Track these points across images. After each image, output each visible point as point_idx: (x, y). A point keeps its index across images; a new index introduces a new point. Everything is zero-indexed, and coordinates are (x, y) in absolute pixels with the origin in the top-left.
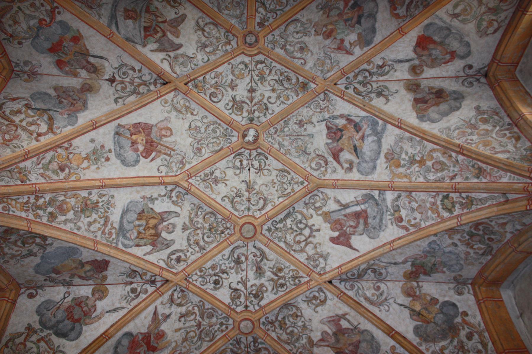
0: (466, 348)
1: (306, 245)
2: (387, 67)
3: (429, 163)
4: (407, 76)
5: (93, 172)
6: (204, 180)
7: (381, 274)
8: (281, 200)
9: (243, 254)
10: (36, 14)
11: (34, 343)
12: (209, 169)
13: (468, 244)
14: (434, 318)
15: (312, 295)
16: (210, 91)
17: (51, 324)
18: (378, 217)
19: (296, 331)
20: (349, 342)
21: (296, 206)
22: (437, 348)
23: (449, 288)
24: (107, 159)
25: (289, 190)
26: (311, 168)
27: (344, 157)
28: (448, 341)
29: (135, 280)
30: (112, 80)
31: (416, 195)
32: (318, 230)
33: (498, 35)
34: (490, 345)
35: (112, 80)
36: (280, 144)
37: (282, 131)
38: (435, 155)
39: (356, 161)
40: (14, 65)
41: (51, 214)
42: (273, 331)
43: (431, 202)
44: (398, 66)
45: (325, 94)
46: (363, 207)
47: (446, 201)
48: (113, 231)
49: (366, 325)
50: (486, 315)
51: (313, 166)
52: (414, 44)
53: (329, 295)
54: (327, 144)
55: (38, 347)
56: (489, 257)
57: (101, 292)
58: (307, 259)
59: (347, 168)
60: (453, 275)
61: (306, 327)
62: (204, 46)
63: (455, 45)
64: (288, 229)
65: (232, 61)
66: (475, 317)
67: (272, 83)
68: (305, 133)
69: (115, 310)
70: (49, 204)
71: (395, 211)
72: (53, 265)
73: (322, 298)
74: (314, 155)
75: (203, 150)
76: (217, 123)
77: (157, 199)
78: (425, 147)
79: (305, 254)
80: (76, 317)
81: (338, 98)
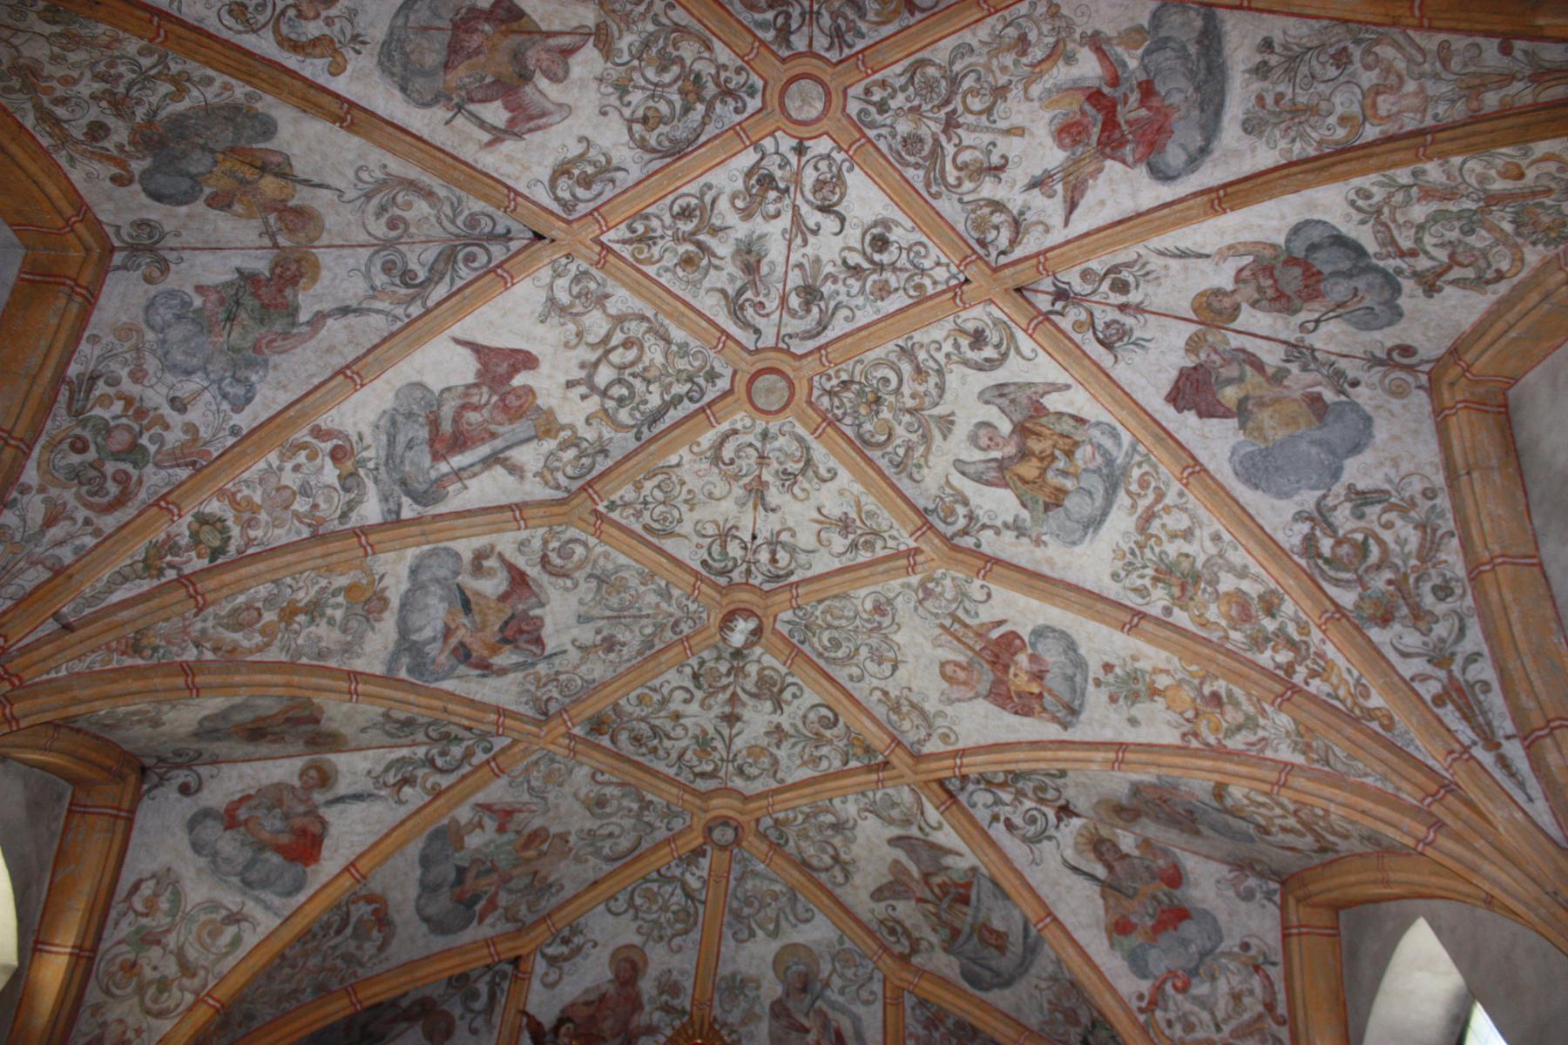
0: (104, 104)
1: (608, 337)
2: (391, 780)
3: (270, 616)
4: (340, 760)
5: (1148, 657)
6: (876, 534)
7: (388, 268)
8: (674, 459)
9: (793, 314)
10: (1188, 1006)
11: (1426, 253)
12: (861, 559)
13: (141, 413)
14: (216, 162)
15: (596, 188)
16: (835, 731)
17: (1370, 277)
18: (399, 449)
19: (651, 73)
20: (482, 58)
21: (633, 445)
22: (195, 93)
23: (178, 235)
24: (1108, 667)
25: (649, 485)
26: (585, 544)
27: (495, 581)
28: (163, 114)
29: (1114, 315)
30: (1065, 811)
31: (298, 532)
32: (570, 384)
33: (127, 879)
34: (29, 122)
35: (1065, 811)
36: (665, 594)
37: (660, 627)
38: (258, 639)
39: (466, 580)
40: (1277, 898)
41: (1271, 611)
42: (725, 67)
43: (257, 526)
44: (366, 785)
45: (545, 714)
46: (444, 468)
47: (217, 543)
48: (1134, 487)
49: (424, 121)
50: (54, 192)
51: (579, 551)
52: (327, 842)
53: (544, 198)
54: (542, 605)
55: (1418, 240)
56: (73, 370)
57: (1213, 311)
58: (607, 296)
59: (487, 557)
60: (171, 282)
61: (617, 87)
62: (838, 827)
63: (228, 844)
64: (657, 379)
65: (774, 785)
66: (89, 177)
67: (680, 732)
68: (601, 623)
69: (1183, 254)
70: (1267, 640)
71: (354, 474)
72: (1317, 434)
73: (563, 182)
74: (576, 575)
75: (869, 605)
76: (827, 660)
77: (1006, 526)
78: (285, 648)
79: (613, 311)
80: (1297, 271)
81: (513, 708)
